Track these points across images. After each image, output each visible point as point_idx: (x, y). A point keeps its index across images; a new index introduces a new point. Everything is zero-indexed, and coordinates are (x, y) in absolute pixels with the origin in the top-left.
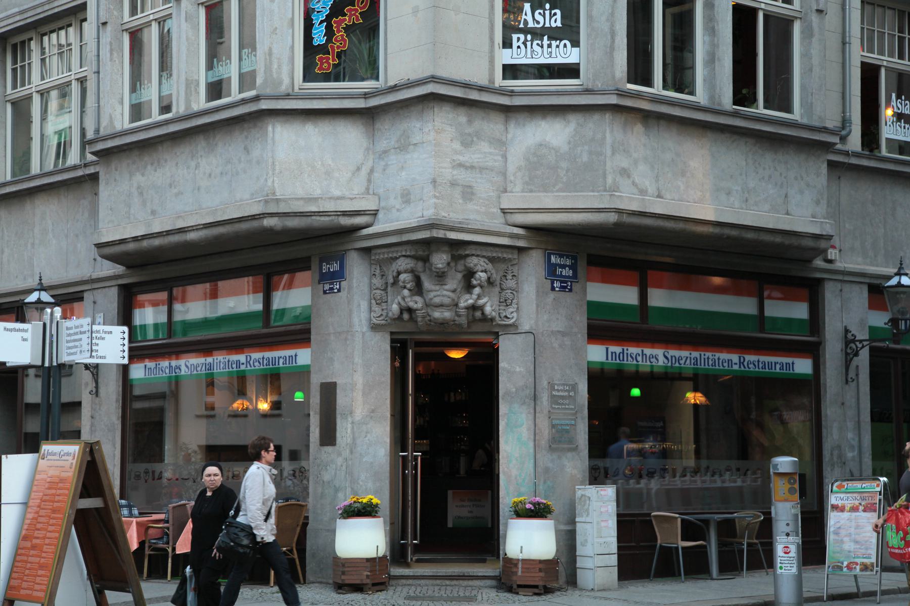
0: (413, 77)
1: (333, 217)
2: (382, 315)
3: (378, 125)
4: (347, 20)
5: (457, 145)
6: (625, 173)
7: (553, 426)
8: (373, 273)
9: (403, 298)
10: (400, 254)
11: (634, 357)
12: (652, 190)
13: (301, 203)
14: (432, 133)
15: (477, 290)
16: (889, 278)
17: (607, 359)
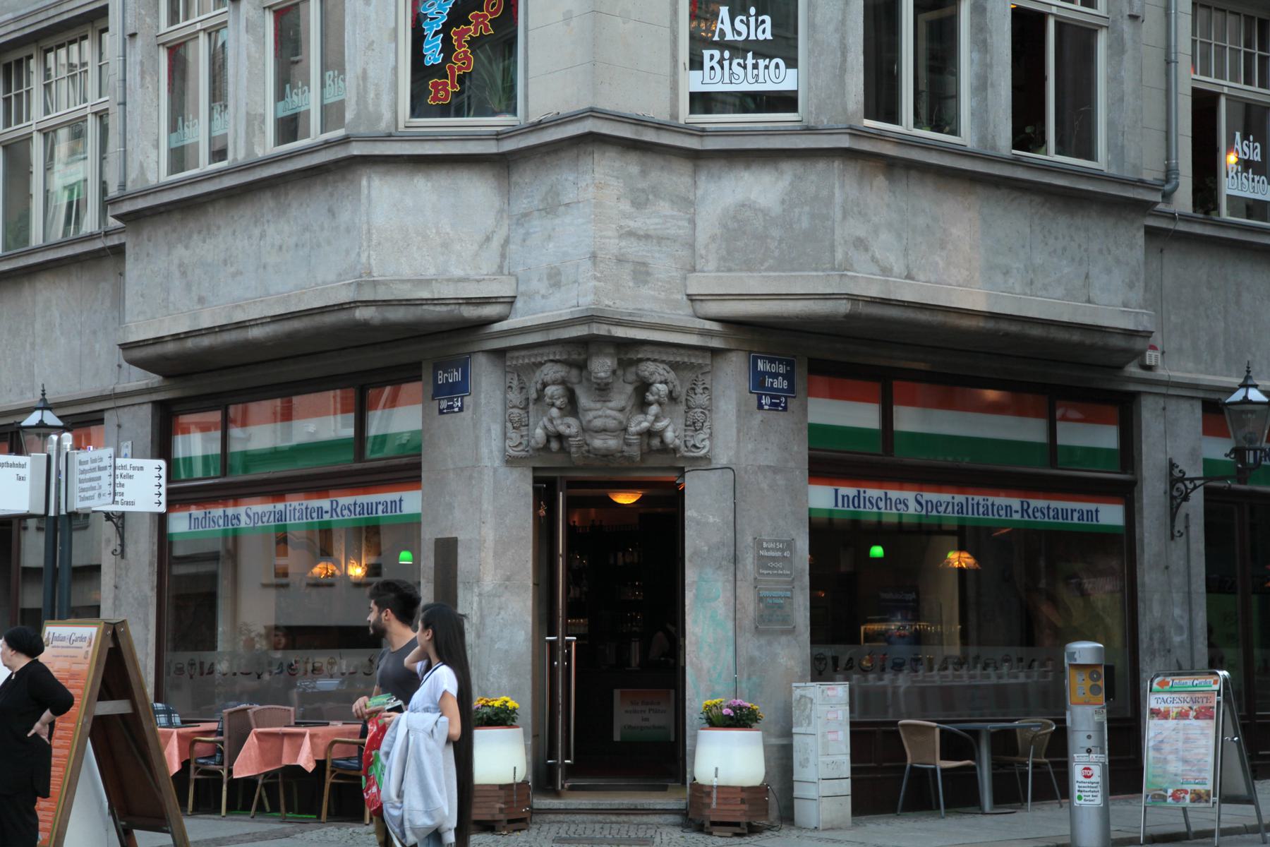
0: (565, 110)
1: (453, 307)
2: (521, 443)
3: (515, 178)
4: (472, 31)
5: (626, 206)
6: (860, 244)
7: (761, 599)
8: (508, 384)
9: (551, 420)
10: (546, 358)
11: (874, 502)
12: (898, 267)
13: (408, 286)
15: (654, 409)
16: (1232, 391)
17: (836, 505)
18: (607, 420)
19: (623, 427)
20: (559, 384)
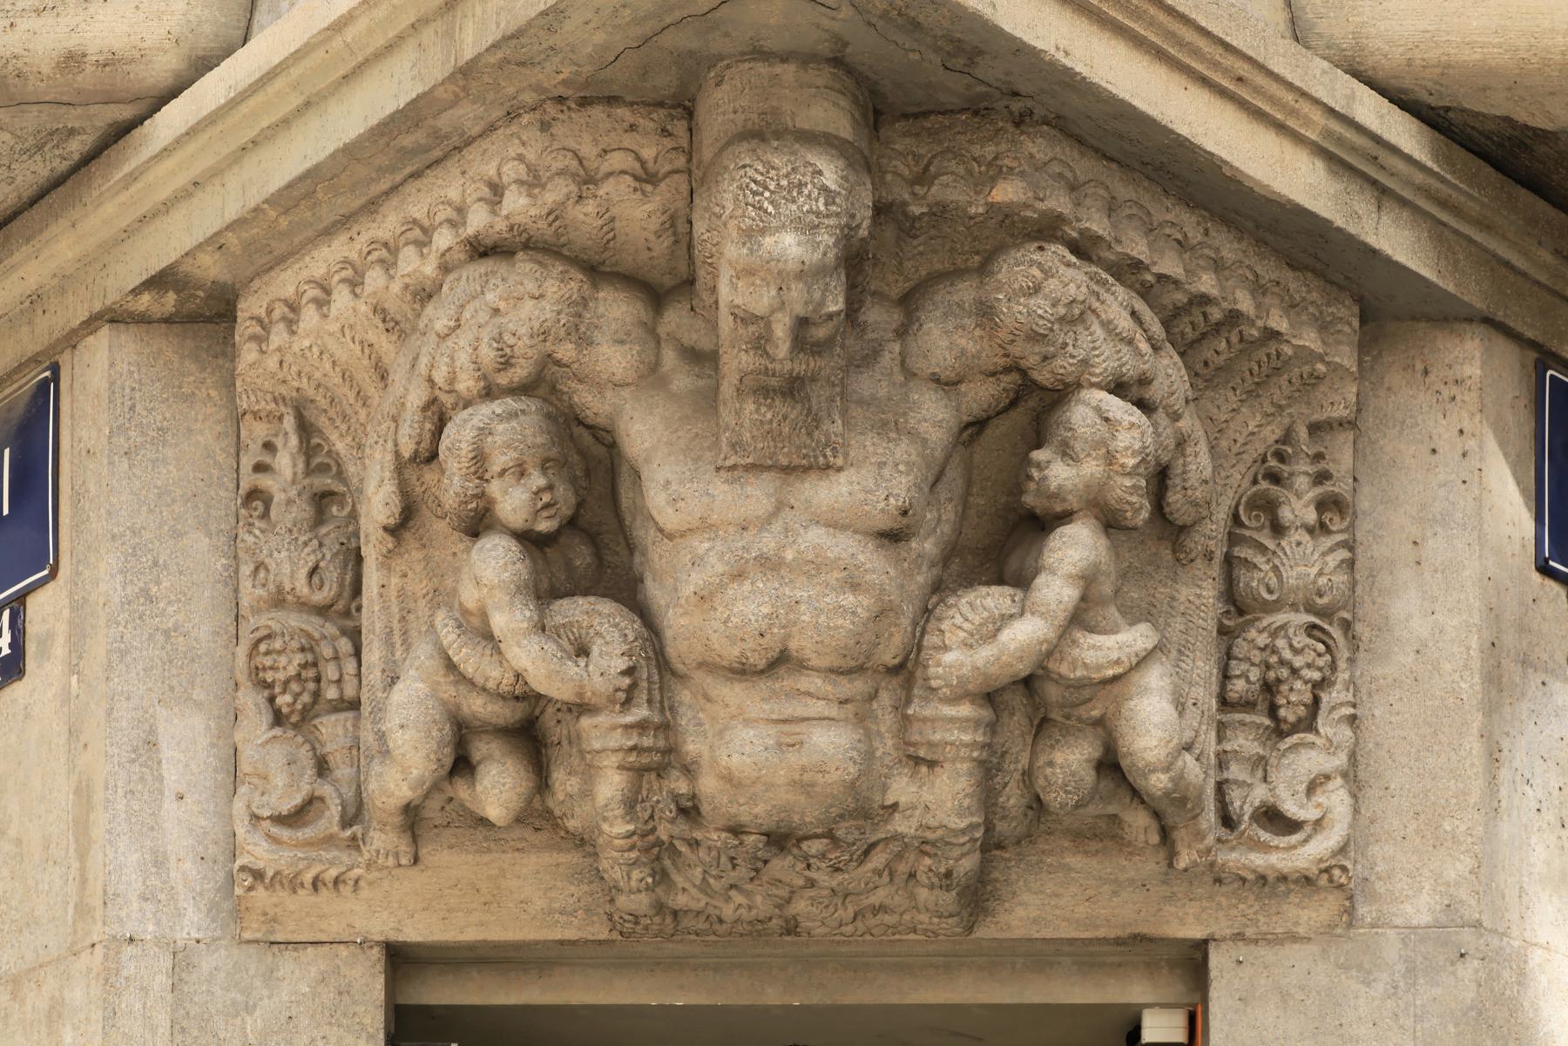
8: (248, 480)
14: (597, 925)
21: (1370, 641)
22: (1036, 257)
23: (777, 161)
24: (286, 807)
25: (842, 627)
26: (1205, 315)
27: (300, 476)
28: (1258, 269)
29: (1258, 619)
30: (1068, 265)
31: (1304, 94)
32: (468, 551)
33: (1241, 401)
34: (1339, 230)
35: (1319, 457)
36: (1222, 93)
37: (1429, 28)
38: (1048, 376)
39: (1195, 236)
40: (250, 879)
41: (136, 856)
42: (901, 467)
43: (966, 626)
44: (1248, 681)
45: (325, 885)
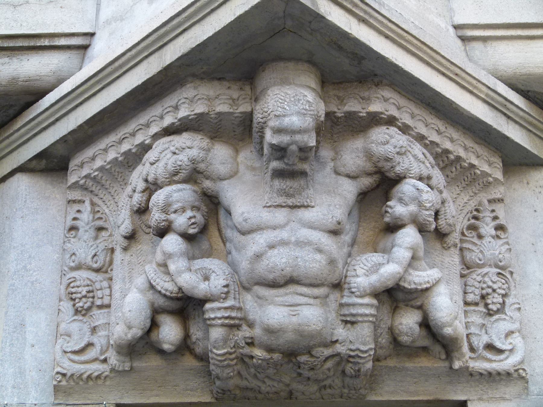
2: (90, 345)
10: (154, 129)
18: (298, 252)
19: (334, 279)
20: (185, 181)
21: (520, 281)
22: (387, 131)
23: (289, 92)
24: (77, 348)
25: (315, 267)
26: (447, 157)
27: (90, 221)
28: (465, 142)
29: (475, 271)
30: (399, 134)
31: (479, 81)
32: (160, 241)
33: (461, 191)
34: (495, 129)
35: (493, 211)
36: (451, 79)
37: (521, 62)
38: (393, 174)
39: (442, 129)
40: (60, 378)
41: (12, 370)
42: (337, 206)
43: (365, 267)
44: (475, 294)
45: (92, 379)
